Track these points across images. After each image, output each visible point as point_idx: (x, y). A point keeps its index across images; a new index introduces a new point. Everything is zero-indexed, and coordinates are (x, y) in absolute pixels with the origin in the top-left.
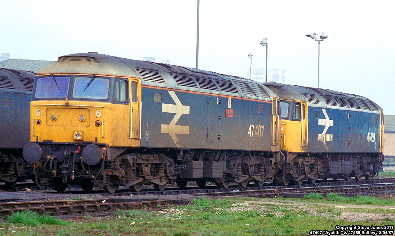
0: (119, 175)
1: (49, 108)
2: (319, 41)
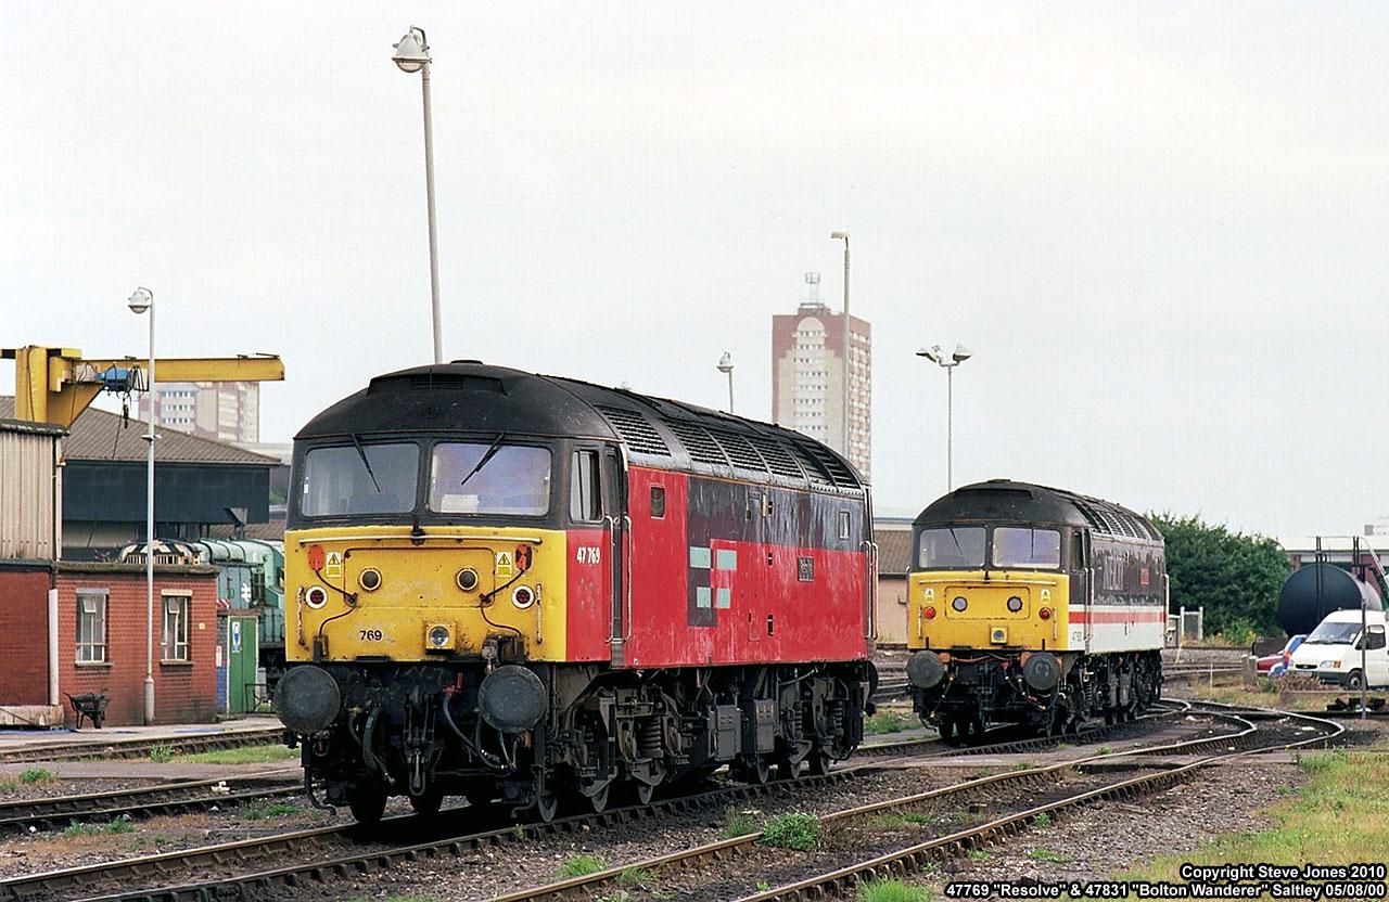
0: (785, 736)
1: (949, 586)
2: (950, 366)
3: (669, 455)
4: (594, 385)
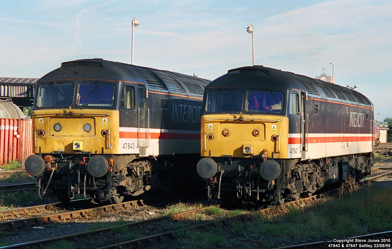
3: (319, 95)
4: (303, 76)
